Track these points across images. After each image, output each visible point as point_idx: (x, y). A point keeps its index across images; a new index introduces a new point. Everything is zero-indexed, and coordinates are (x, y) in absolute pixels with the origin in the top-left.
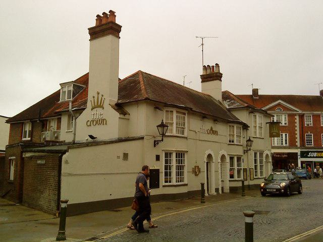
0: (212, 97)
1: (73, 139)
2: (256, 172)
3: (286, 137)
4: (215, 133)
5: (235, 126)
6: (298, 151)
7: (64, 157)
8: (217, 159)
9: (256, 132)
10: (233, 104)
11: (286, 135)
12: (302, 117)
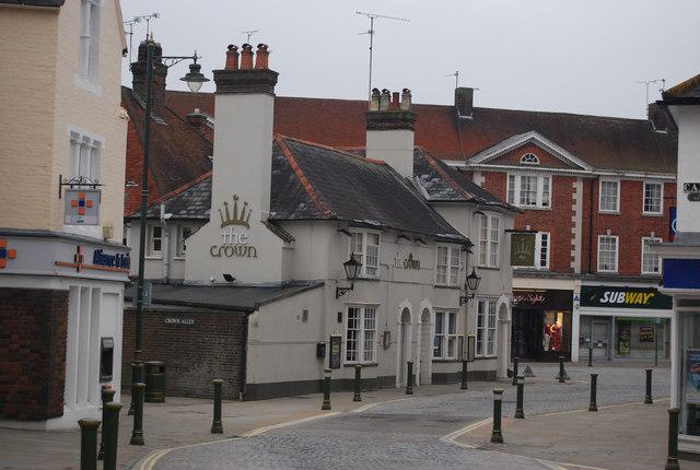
0: (390, 168)
1: (165, 275)
2: (479, 345)
3: (544, 244)
4: (413, 264)
5: (450, 247)
6: (575, 286)
7: (251, 318)
8: (416, 318)
9: (484, 256)
10: (439, 187)
11: (544, 237)
12: (591, 184)
